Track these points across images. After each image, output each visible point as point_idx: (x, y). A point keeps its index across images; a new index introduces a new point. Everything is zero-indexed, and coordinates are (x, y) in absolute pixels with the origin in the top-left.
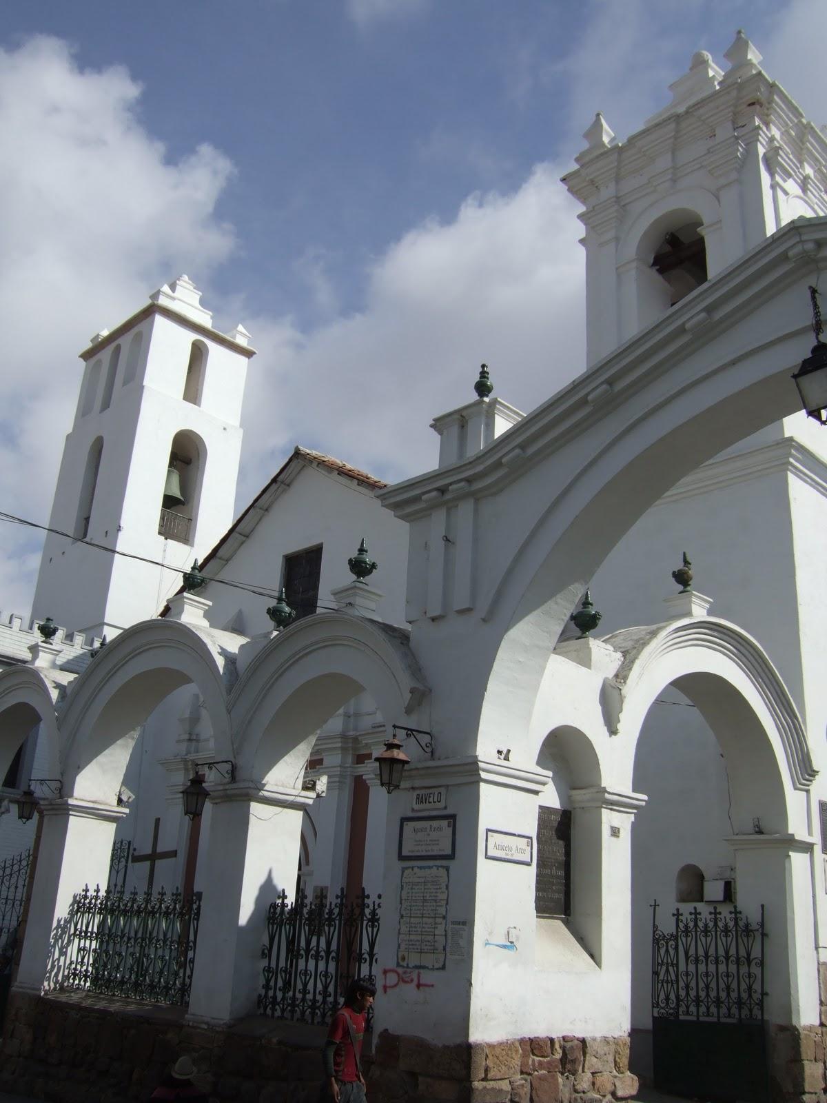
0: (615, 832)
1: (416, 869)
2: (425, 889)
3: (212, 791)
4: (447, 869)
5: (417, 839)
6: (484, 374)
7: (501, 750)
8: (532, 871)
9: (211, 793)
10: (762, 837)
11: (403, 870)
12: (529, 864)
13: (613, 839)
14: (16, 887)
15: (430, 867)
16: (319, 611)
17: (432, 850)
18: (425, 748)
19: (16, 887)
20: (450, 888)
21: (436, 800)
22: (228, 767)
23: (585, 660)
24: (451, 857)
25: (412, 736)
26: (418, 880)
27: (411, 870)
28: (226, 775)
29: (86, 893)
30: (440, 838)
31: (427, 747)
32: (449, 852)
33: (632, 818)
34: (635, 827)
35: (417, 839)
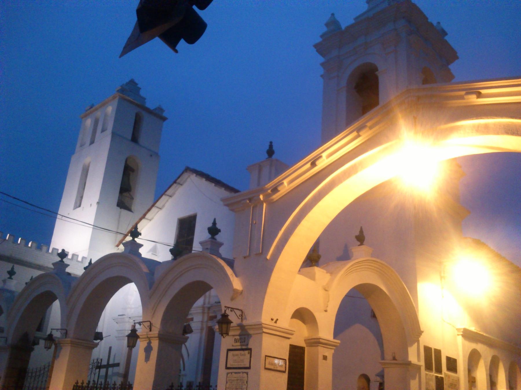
0: (325, 358)
1: (233, 373)
2: (237, 383)
3: (141, 335)
4: (247, 373)
5: (234, 359)
6: (271, 146)
7: (273, 318)
8: (285, 376)
9: (140, 336)
10: (395, 362)
11: (228, 374)
12: (284, 372)
13: (324, 361)
14: (42, 382)
15: (239, 373)
16: (193, 252)
17: (241, 365)
18: (239, 317)
19: (42, 382)
20: (248, 383)
21: (243, 341)
22: (149, 324)
23: (312, 277)
24: (249, 368)
25: (233, 311)
26: (233, 379)
27: (230, 374)
28: (147, 328)
29: (77, 384)
30: (243, 358)
31: (240, 316)
32: (248, 366)
33: (333, 351)
34: (334, 356)
35: (234, 359)
